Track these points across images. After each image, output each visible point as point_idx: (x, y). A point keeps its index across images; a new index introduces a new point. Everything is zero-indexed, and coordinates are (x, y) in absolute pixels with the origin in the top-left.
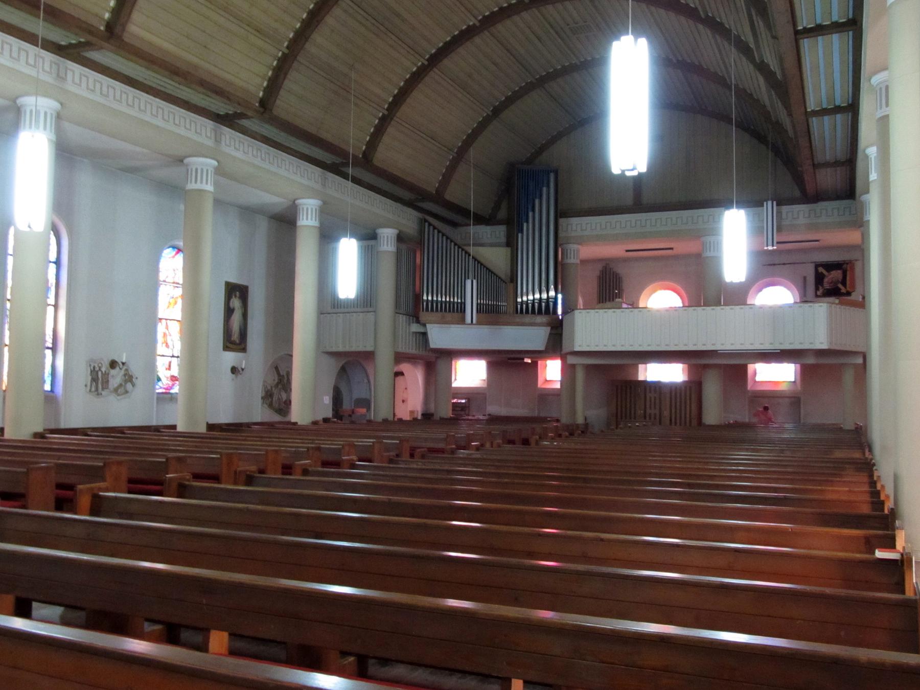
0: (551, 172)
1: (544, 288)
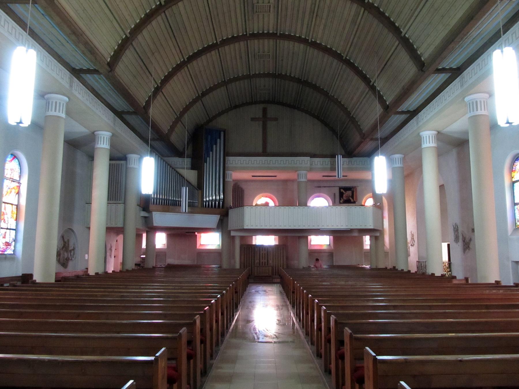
1: (217, 193)
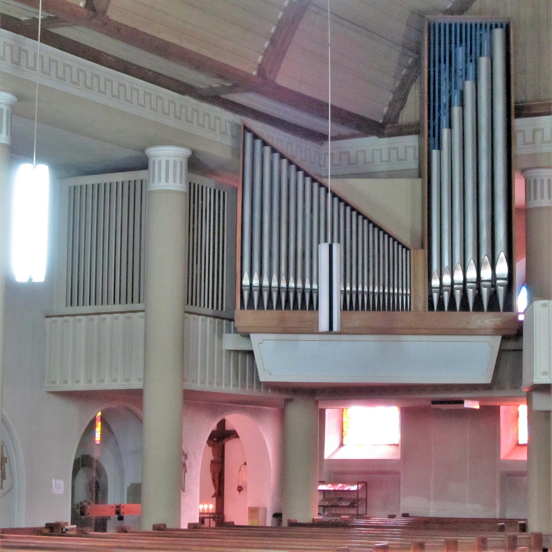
0: (496, 27)
1: (485, 259)
